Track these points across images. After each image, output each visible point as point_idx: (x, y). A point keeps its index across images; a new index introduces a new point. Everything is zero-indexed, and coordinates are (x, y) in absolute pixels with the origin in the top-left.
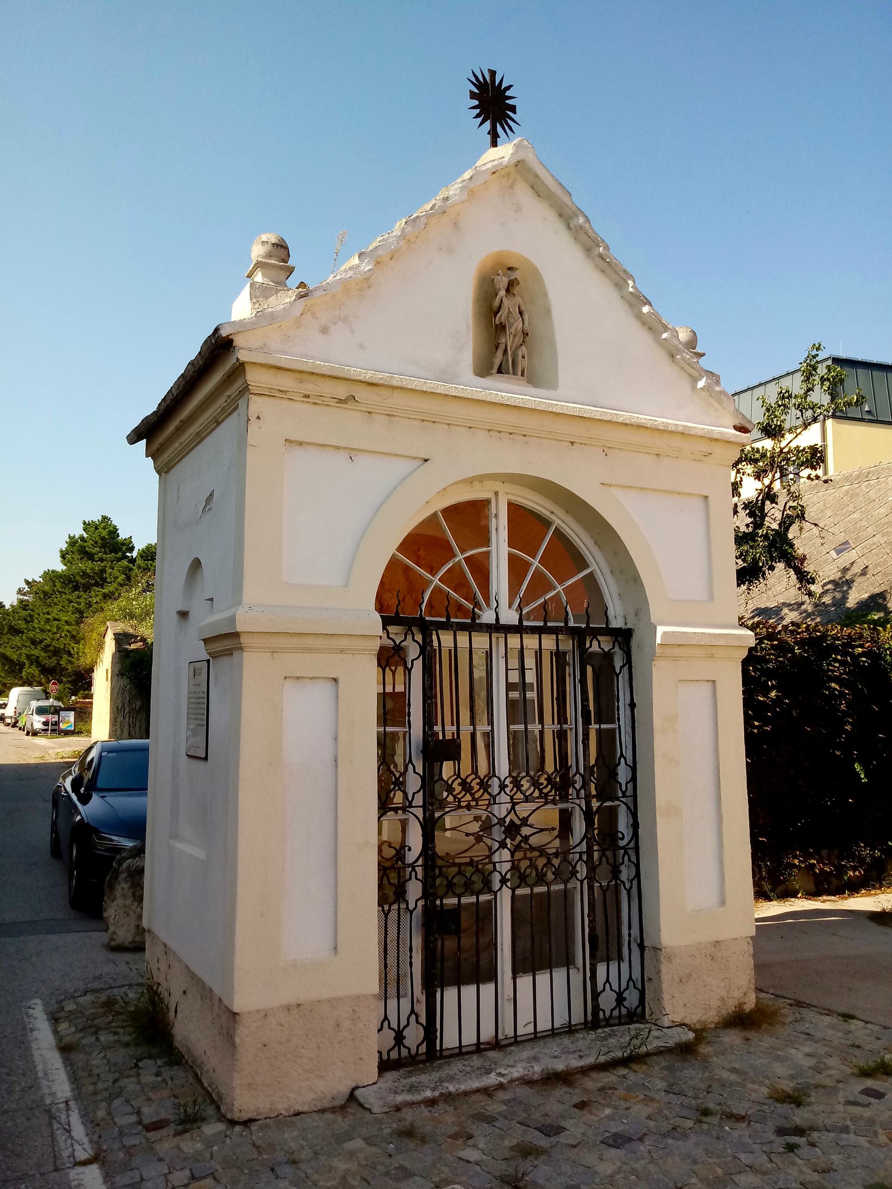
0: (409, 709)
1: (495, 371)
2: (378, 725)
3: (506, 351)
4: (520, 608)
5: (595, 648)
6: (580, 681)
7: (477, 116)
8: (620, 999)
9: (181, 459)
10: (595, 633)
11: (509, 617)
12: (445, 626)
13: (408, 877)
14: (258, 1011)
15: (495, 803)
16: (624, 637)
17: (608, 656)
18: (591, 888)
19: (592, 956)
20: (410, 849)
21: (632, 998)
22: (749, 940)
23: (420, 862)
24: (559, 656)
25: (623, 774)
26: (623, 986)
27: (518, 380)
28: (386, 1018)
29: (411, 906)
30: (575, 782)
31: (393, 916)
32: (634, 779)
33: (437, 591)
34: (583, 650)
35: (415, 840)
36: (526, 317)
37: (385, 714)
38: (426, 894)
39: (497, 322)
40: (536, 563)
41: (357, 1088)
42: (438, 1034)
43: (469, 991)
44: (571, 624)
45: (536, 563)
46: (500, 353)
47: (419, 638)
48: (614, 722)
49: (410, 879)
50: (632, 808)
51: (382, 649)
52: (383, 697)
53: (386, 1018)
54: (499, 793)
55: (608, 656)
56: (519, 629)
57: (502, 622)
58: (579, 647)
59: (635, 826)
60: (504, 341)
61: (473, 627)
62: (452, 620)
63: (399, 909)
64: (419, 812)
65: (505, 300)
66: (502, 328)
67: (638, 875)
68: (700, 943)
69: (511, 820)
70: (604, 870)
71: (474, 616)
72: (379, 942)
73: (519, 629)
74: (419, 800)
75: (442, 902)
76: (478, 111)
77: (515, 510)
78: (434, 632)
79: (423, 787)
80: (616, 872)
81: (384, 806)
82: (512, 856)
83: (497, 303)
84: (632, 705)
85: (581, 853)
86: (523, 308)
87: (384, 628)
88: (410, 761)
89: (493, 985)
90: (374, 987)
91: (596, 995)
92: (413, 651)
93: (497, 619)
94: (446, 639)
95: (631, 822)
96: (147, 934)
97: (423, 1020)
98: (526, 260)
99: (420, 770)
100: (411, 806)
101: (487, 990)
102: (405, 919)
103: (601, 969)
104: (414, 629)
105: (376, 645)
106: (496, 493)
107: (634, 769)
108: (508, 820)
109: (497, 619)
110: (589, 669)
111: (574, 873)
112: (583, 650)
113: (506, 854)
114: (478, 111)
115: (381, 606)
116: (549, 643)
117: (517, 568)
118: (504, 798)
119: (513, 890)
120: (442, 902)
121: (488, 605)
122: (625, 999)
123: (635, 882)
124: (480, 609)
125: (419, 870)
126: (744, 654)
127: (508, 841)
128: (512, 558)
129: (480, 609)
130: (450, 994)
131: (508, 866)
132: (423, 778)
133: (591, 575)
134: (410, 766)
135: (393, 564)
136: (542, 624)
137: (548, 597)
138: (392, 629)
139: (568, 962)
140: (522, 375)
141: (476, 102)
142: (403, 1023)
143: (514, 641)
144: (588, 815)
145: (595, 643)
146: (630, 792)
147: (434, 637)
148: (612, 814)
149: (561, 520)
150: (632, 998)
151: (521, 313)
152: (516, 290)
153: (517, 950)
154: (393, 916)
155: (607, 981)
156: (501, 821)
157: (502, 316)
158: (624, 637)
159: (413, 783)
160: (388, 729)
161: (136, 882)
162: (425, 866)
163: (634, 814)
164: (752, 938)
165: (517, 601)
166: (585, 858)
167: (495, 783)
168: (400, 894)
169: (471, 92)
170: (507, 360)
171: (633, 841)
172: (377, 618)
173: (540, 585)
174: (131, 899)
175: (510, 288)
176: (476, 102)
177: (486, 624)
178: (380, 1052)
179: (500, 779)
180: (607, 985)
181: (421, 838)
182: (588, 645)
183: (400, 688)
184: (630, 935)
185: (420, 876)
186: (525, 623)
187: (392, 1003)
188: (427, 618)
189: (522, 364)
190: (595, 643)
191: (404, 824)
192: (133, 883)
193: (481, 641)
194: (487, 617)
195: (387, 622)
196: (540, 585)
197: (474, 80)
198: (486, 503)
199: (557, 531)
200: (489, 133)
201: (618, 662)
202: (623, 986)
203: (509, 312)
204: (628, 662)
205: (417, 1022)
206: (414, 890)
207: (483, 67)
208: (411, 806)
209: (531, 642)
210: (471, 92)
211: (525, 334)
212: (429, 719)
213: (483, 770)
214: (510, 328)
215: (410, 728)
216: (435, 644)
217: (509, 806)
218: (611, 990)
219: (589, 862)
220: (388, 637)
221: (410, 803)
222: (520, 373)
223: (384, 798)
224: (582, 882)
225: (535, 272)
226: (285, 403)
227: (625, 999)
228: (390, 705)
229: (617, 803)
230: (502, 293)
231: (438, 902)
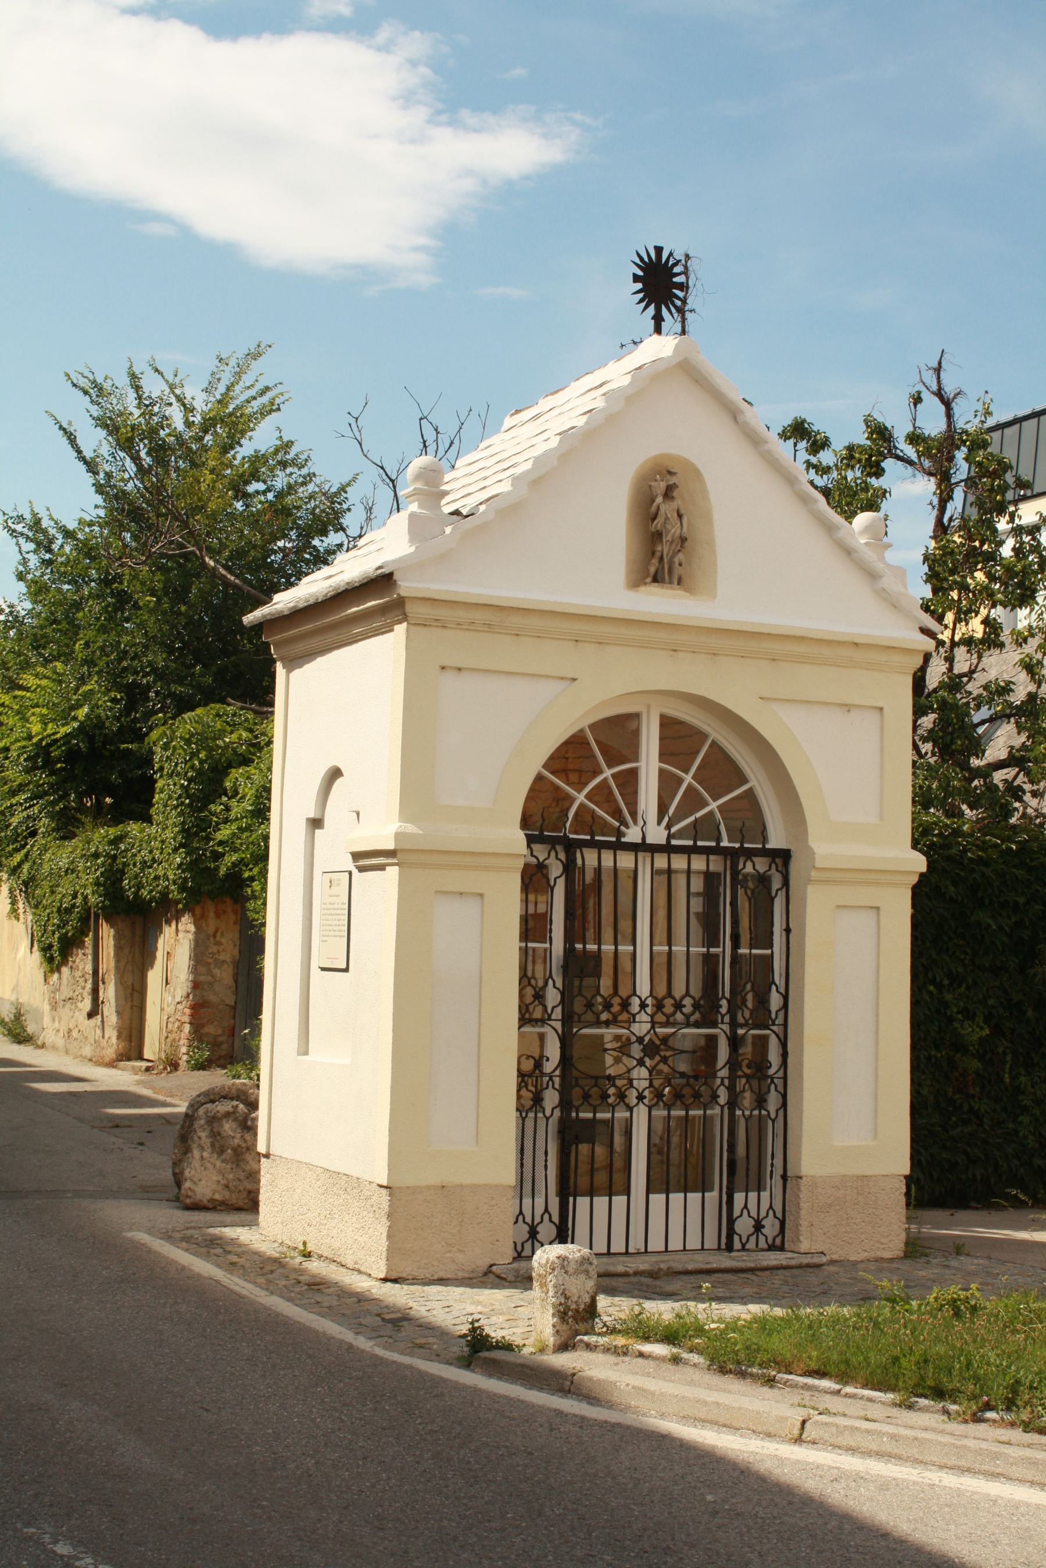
0: (551, 924)
1: (649, 580)
2: (521, 941)
3: (661, 559)
4: (668, 827)
5: (749, 869)
6: (731, 904)
7: (641, 301)
8: (758, 1227)
9: (465, 853)
10: (750, 854)
11: (657, 835)
12: (592, 844)
13: (545, 1086)
14: (408, 1188)
15: (634, 1022)
16: (783, 856)
17: (764, 880)
18: (732, 1115)
19: (730, 1182)
20: (548, 1060)
21: (771, 1228)
22: (902, 1178)
23: (557, 1072)
24: (710, 877)
25: (775, 1001)
26: (763, 1214)
27: (672, 589)
28: (521, 1213)
29: (548, 1113)
30: (721, 1006)
31: (529, 1123)
32: (785, 1006)
33: (582, 806)
34: (735, 873)
35: (553, 1051)
36: (685, 520)
37: (527, 930)
38: (565, 1104)
39: (653, 530)
40: (688, 779)
41: (494, 1265)
42: (570, 1232)
43: (601, 1202)
44: (725, 843)
45: (688, 779)
46: (655, 561)
47: (562, 856)
48: (718, 947)
49: (547, 1087)
50: (782, 1036)
51: (527, 866)
52: (525, 919)
53: (521, 1213)
54: (639, 1012)
55: (764, 880)
56: (667, 849)
57: (649, 841)
58: (732, 868)
59: (785, 1055)
60: (659, 548)
61: (619, 846)
62: (597, 838)
63: (536, 1117)
64: (558, 1025)
65: (663, 508)
66: (657, 536)
67: (784, 1105)
68: (845, 1176)
69: (650, 1040)
70: (747, 1099)
71: (620, 834)
72: (517, 1127)
73: (667, 849)
74: (558, 1013)
75: (577, 1114)
76: (641, 295)
77: (667, 724)
78: (578, 851)
79: (562, 1001)
80: (761, 1102)
81: (524, 1020)
82: (650, 1075)
83: (653, 509)
84: (788, 930)
85: (722, 1079)
86: (682, 511)
87: (529, 846)
88: (551, 976)
89: (626, 1197)
90: (509, 1176)
91: (731, 1221)
92: (555, 869)
93: (644, 838)
94: (590, 858)
95: (781, 1051)
96: (263, 1160)
97: (556, 1218)
98: (687, 460)
99: (559, 984)
100: (550, 1019)
101: (619, 1201)
102: (541, 1123)
103: (739, 1198)
104: (559, 848)
105: (520, 864)
106: (649, 706)
107: (786, 998)
108: (647, 1039)
109: (644, 838)
110: (740, 892)
111: (715, 1097)
112: (735, 873)
113: (644, 1072)
114: (641, 295)
115: (525, 822)
116: (699, 863)
117: (667, 784)
118: (643, 1017)
119: (650, 1108)
120: (577, 1114)
121: (635, 822)
122: (763, 1227)
123: (781, 1112)
124: (627, 827)
125: (557, 1080)
126: (915, 879)
127: (647, 1060)
128: (662, 772)
129: (627, 827)
130: (583, 1202)
131: (646, 1084)
132: (562, 993)
133: (751, 791)
134: (550, 982)
135: (539, 778)
136: (691, 843)
137: (699, 814)
138: (536, 847)
139: (704, 1187)
140: (679, 584)
141: (639, 286)
142: (537, 1220)
143: (661, 861)
144: (735, 1042)
145: (749, 864)
146: (780, 1020)
147: (578, 855)
148: (762, 1043)
149: (717, 732)
150: (771, 1228)
151: (680, 516)
152: (675, 494)
153: (652, 1173)
154: (529, 1123)
155: (746, 1206)
156: (640, 1040)
157: (659, 522)
158: (783, 856)
159: (552, 997)
160: (530, 945)
161: (215, 1130)
162: (563, 1077)
163: (784, 1044)
164: (906, 1177)
165: (666, 819)
166: (726, 1082)
167: (635, 1002)
168: (538, 1100)
169: (635, 275)
170: (663, 568)
171: (782, 1070)
172: (520, 836)
173: (693, 801)
174: (209, 1150)
175: (669, 493)
176: (639, 286)
177: (632, 844)
178: (515, 1243)
179: (640, 998)
180: (745, 1211)
181: (558, 1051)
182: (741, 866)
183: (542, 908)
184: (772, 1165)
185: (557, 1086)
186: (674, 842)
187: (527, 1202)
188: (572, 836)
189: (678, 571)
190: (749, 864)
191: (542, 1037)
192: (212, 1131)
193: (626, 860)
194: (632, 835)
195: (531, 840)
196: (693, 801)
197: (638, 261)
198: (637, 716)
199: (714, 744)
200: (653, 318)
201: (776, 883)
202: (763, 1214)
203: (667, 518)
204: (786, 883)
205: (551, 1220)
206: (551, 1098)
207: (645, 244)
208: (550, 1019)
209: (679, 862)
210: (635, 275)
211: (683, 540)
212: (570, 937)
213: (624, 992)
214: (667, 535)
215: (551, 944)
216: (579, 862)
217: (649, 1026)
218: (749, 1216)
219: (731, 1089)
220: (532, 855)
221: (550, 1016)
222: (676, 581)
223: (523, 1011)
224: (722, 1107)
225: (696, 473)
226: (440, 630)
227: (763, 1227)
228: (531, 924)
229: (767, 1032)
230: (659, 500)
231: (574, 1114)
